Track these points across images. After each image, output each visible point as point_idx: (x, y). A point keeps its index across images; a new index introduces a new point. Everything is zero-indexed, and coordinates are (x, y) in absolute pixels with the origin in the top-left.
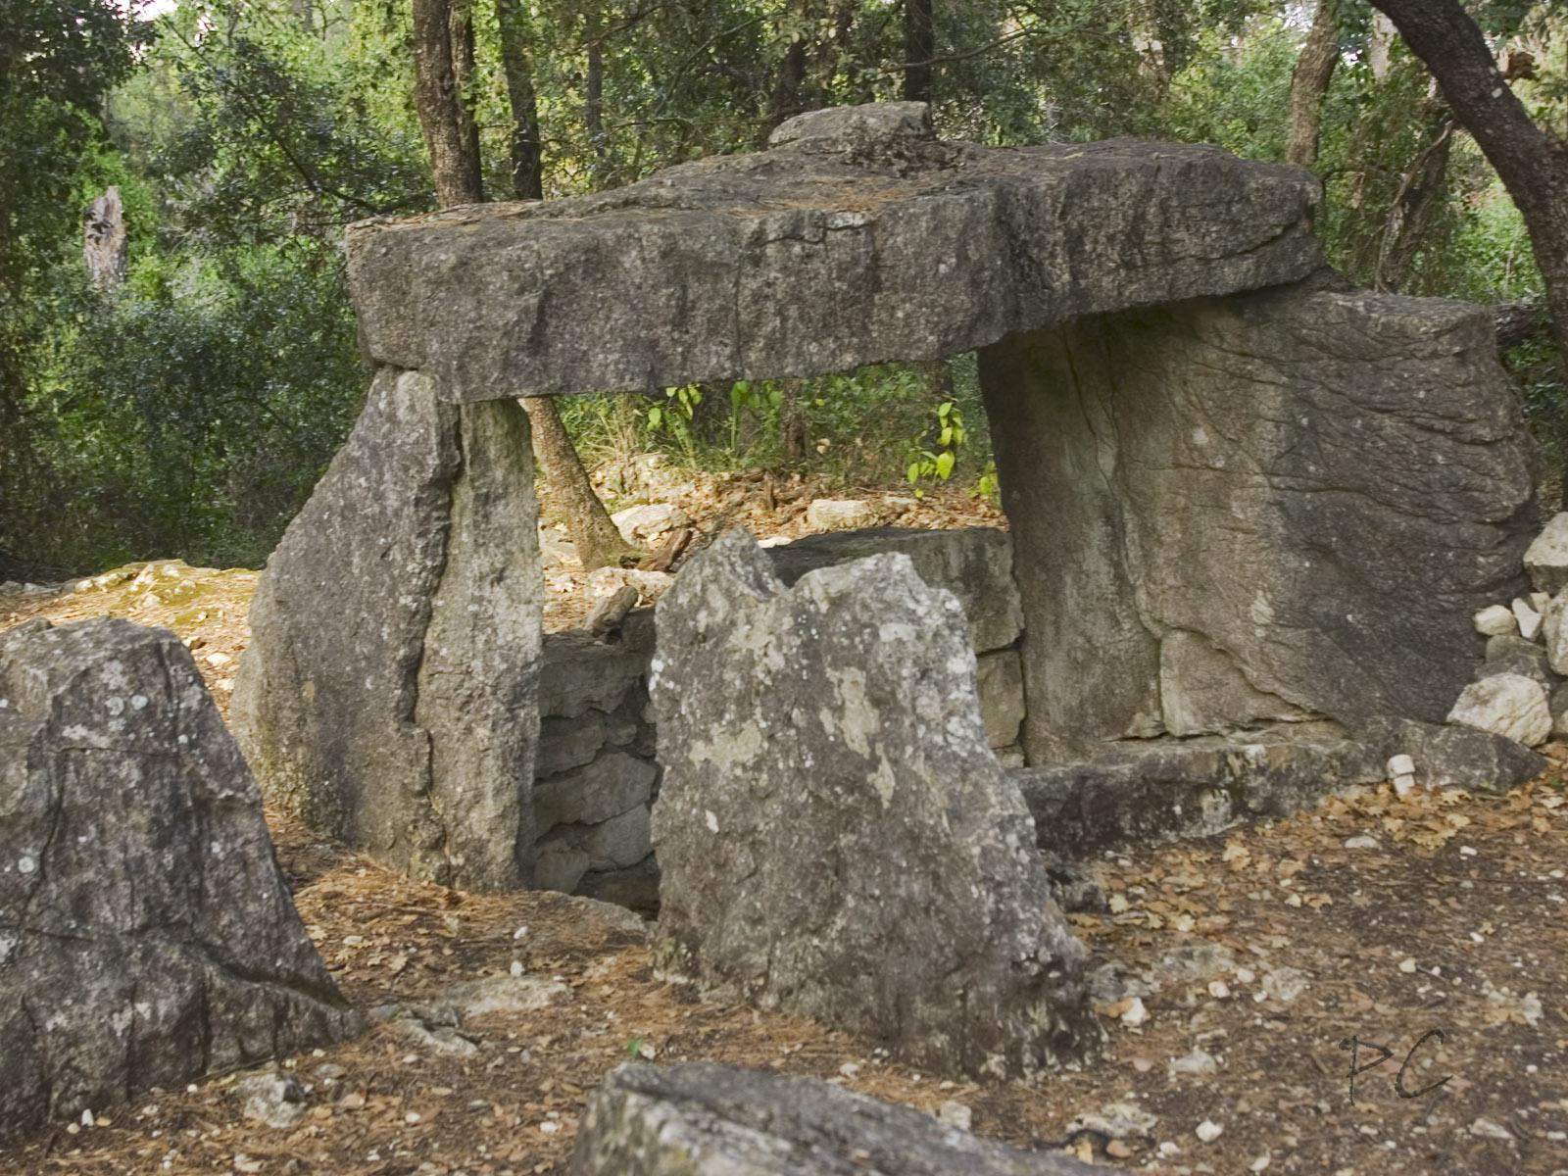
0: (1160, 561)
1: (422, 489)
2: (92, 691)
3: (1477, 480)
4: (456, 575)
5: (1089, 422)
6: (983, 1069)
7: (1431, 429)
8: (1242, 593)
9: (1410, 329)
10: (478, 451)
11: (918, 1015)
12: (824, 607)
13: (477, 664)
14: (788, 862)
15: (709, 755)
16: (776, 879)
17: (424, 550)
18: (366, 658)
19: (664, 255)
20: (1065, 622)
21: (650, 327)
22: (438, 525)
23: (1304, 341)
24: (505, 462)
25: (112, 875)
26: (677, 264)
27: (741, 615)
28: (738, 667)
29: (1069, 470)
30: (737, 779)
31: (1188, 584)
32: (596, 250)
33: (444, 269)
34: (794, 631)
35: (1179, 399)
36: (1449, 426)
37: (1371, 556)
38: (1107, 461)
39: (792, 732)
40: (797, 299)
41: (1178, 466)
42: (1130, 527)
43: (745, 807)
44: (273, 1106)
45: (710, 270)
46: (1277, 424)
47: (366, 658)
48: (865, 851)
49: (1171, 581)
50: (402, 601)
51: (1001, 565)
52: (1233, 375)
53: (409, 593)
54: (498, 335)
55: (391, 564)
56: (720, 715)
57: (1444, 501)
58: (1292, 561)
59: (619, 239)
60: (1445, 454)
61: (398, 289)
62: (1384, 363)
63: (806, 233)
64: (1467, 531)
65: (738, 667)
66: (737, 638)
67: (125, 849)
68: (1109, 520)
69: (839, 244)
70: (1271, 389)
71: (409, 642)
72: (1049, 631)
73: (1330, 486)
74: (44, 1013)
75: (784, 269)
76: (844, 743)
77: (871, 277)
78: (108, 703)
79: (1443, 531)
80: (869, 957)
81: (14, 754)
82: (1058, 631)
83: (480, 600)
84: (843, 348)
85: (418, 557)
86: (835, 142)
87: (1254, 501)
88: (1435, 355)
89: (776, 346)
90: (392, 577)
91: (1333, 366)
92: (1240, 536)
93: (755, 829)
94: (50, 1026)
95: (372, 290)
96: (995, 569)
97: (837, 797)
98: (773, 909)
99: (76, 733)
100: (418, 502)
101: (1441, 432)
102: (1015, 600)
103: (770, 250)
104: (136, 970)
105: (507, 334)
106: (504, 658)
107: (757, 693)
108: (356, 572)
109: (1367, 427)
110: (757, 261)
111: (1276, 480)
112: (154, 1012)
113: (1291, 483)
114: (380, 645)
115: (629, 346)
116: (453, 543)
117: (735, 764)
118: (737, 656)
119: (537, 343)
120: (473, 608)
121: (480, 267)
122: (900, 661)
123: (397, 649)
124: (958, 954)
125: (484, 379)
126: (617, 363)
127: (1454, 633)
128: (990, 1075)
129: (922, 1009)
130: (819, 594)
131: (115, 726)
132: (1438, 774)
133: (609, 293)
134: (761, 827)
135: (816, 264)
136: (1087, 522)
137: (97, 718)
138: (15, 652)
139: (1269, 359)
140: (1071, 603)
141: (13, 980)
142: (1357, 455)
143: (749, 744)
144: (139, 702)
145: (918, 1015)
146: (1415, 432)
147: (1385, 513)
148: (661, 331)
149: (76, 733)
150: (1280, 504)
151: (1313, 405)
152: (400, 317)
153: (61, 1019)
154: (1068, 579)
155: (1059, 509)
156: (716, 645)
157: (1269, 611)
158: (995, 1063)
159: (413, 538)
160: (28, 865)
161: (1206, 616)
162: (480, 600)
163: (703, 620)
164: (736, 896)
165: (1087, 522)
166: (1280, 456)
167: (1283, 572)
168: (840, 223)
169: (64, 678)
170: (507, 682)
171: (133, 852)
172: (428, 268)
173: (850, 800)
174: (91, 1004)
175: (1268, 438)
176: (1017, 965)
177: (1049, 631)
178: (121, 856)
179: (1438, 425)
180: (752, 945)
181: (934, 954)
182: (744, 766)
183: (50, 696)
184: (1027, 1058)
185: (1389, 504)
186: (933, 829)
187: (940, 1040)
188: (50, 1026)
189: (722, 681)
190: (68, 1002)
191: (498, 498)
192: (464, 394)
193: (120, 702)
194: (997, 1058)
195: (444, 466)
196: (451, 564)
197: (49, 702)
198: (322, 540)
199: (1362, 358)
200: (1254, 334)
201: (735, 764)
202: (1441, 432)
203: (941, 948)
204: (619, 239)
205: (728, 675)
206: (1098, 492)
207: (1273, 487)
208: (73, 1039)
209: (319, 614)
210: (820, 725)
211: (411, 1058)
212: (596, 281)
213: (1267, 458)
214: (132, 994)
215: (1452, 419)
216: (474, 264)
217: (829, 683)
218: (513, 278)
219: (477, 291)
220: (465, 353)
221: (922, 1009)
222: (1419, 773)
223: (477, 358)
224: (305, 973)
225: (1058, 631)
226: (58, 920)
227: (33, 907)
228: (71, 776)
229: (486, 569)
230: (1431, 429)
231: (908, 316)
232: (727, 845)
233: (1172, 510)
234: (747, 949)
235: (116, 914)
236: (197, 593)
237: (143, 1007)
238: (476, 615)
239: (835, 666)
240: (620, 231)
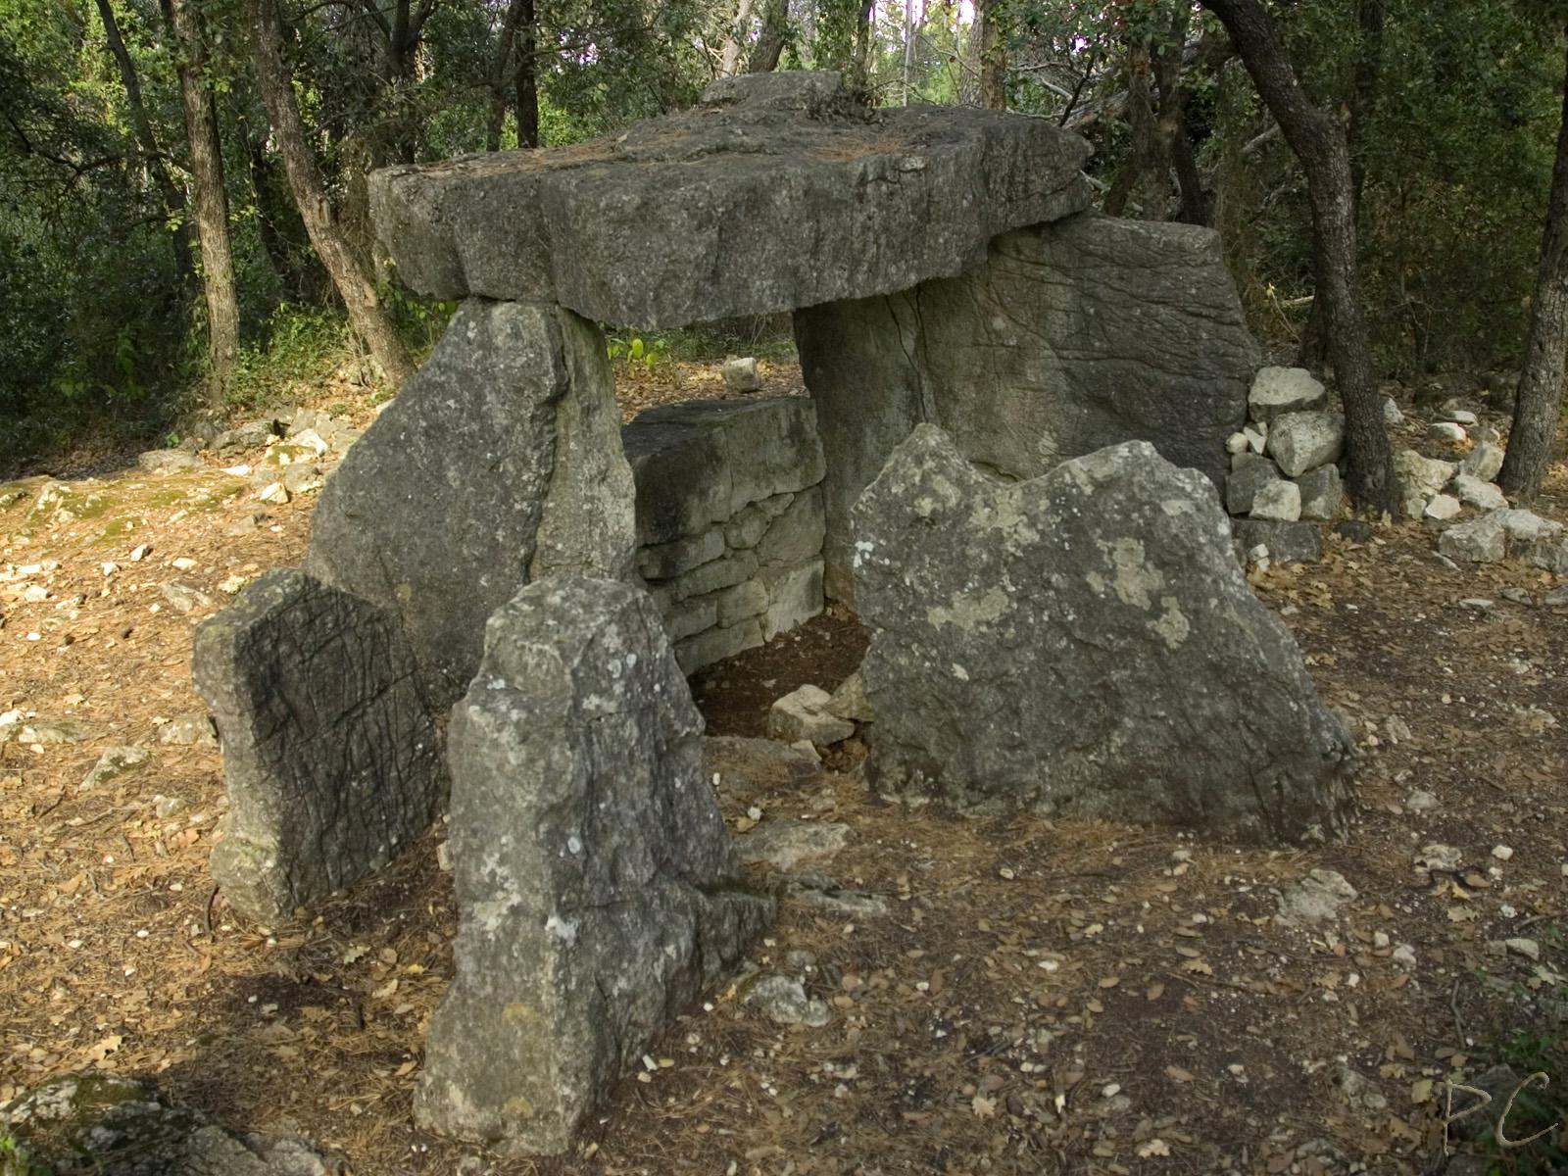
0: (956, 414)
1: (537, 407)
2: (597, 657)
3: (1232, 349)
4: (564, 479)
5: (894, 316)
6: (1304, 837)
7: (1200, 315)
8: (1032, 434)
9: (1187, 246)
10: (579, 370)
11: (1230, 804)
12: (1088, 490)
13: (595, 554)
14: (1046, 696)
15: (949, 618)
16: (1035, 711)
17: (539, 461)
18: (477, 559)
19: (806, 193)
20: (865, 462)
21: (793, 257)
22: (550, 437)
23: (1090, 254)
24: (596, 378)
25: (631, 834)
26: (816, 202)
27: (978, 499)
28: (984, 543)
29: (873, 350)
30: (983, 635)
31: (981, 429)
32: (753, 190)
33: (629, 209)
34: (1053, 509)
35: (981, 297)
36: (1213, 313)
37: (1146, 404)
38: (909, 343)
39: (1051, 593)
40: (886, 229)
41: (976, 344)
42: (926, 390)
43: (993, 656)
44: (800, 1008)
45: (835, 206)
46: (1067, 312)
47: (477, 559)
48: (1141, 683)
49: (965, 428)
50: (518, 507)
51: (811, 422)
52: (1028, 278)
53: (524, 499)
54: (691, 267)
55: (501, 476)
56: (963, 585)
57: (1205, 363)
58: (1074, 410)
59: (773, 179)
60: (1208, 332)
61: (500, 229)
62: (1162, 269)
63: (889, 175)
64: (1222, 384)
65: (984, 543)
66: (980, 516)
67: (633, 806)
68: (909, 386)
69: (911, 184)
70: (1060, 289)
71: (525, 542)
72: (850, 470)
73: (1111, 355)
74: (610, 981)
75: (879, 205)
76: (1117, 598)
77: (926, 211)
78: (610, 667)
79: (1204, 385)
80: (1156, 764)
81: (551, 737)
82: (858, 469)
83: (591, 499)
84: (909, 269)
85: (534, 467)
86: (794, 101)
87: (1045, 368)
88: (1205, 263)
89: (873, 271)
90: (504, 487)
91: (1116, 271)
92: (1029, 393)
93: (1006, 673)
94: (616, 992)
95: (473, 230)
96: (807, 427)
97: (1110, 642)
98: (1034, 736)
99: (591, 702)
100: (533, 418)
101: (1208, 317)
102: (820, 448)
103: (869, 189)
104: (660, 917)
105: (698, 267)
106: (615, 547)
107: (1006, 564)
108: (456, 484)
109: (1144, 314)
110: (861, 198)
111: (1065, 353)
112: (678, 949)
113: (1077, 354)
114: (494, 546)
115: (782, 272)
116: (562, 450)
117: (978, 623)
118: (981, 534)
119: (715, 276)
120: (586, 507)
121: (659, 207)
122: (1191, 530)
123: (516, 549)
124: (1270, 754)
125: (677, 307)
126: (771, 288)
127: (1209, 454)
128: (1312, 840)
129: (1232, 799)
130: (1082, 478)
131: (618, 688)
132: (1282, 555)
133: (763, 228)
134: (1013, 671)
135: (897, 200)
136: (890, 388)
137: (604, 683)
138: (502, 628)
139: (1057, 267)
140: (870, 449)
141: (584, 960)
142: (1136, 335)
143: (996, 604)
144: (632, 659)
145: (1230, 804)
146: (1182, 316)
147: (1158, 373)
148: (802, 260)
149: (591, 702)
150: (1067, 371)
151: (1098, 299)
152: (502, 254)
153: (622, 983)
154: (868, 431)
155: (862, 379)
156: (954, 526)
157: (1053, 445)
158: (1316, 831)
159: (529, 451)
160: (575, 845)
161: (997, 451)
162: (591, 499)
163: (926, 505)
164: (983, 730)
165: (890, 388)
166: (1070, 335)
167: (1067, 417)
168: (908, 166)
169: (575, 650)
170: (617, 566)
171: (640, 807)
172: (609, 207)
173: (1122, 643)
174: (640, 960)
175: (1060, 324)
176: (1326, 756)
177: (850, 470)
178: (632, 813)
179: (1205, 312)
180: (1017, 767)
181: (1245, 757)
182: (989, 624)
183: (567, 671)
184: (1334, 823)
185: (1161, 367)
186: (1248, 662)
187: (1251, 820)
188: (616, 992)
189: (964, 556)
190: (625, 965)
191: (596, 408)
192: (659, 321)
193: (618, 663)
194: (1317, 827)
195: (559, 385)
196: (559, 470)
197: (568, 677)
198: (402, 458)
199: (1142, 266)
200: (1047, 249)
201: (978, 623)
202: (1208, 317)
203: (1252, 752)
204: (773, 179)
205: (972, 551)
206: (901, 366)
207: (1060, 357)
208: (631, 997)
209: (411, 524)
210: (1087, 587)
211: (849, 928)
212: (754, 217)
213: (1058, 338)
214: (661, 942)
215: (1215, 308)
216: (653, 205)
217: (1099, 552)
218: (692, 216)
219: (661, 228)
220: (661, 285)
221: (1232, 799)
222: (1271, 556)
223: (670, 290)
224: (734, 875)
225: (858, 469)
226: (603, 891)
227: (587, 885)
228: (596, 747)
229: (594, 472)
230: (1200, 315)
231: (946, 242)
232: (976, 689)
233: (969, 377)
234: (1011, 771)
235: (636, 871)
236: (106, 507)
237: (670, 949)
238: (590, 512)
239: (1106, 537)
240: (773, 172)
